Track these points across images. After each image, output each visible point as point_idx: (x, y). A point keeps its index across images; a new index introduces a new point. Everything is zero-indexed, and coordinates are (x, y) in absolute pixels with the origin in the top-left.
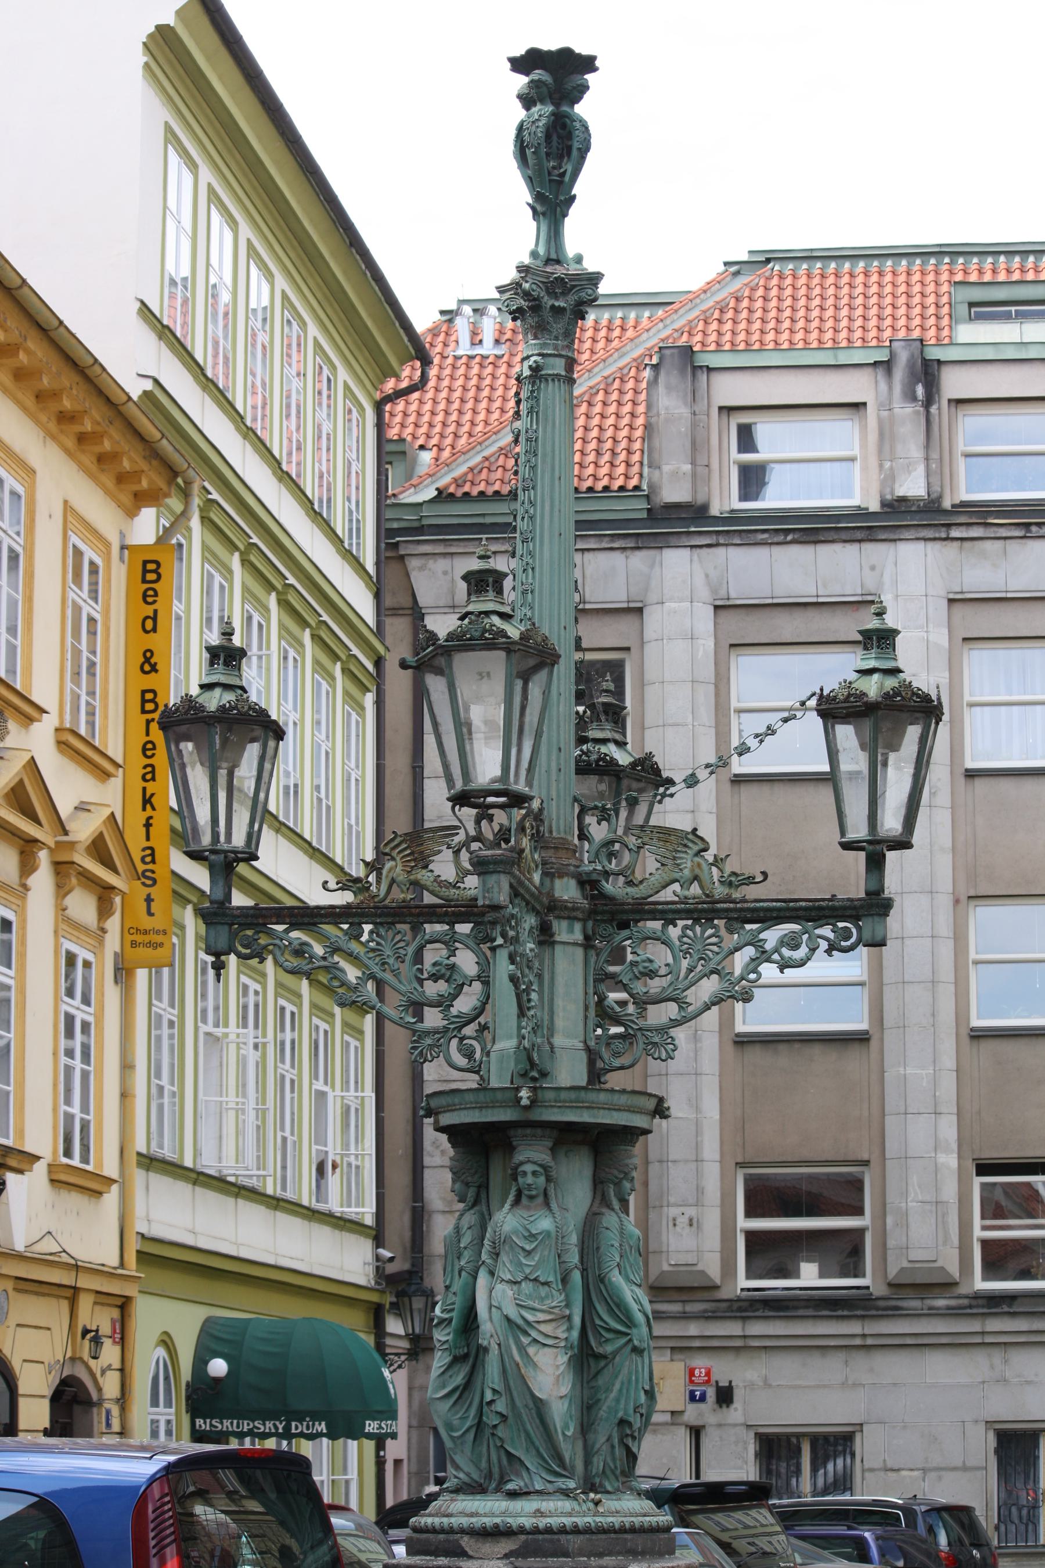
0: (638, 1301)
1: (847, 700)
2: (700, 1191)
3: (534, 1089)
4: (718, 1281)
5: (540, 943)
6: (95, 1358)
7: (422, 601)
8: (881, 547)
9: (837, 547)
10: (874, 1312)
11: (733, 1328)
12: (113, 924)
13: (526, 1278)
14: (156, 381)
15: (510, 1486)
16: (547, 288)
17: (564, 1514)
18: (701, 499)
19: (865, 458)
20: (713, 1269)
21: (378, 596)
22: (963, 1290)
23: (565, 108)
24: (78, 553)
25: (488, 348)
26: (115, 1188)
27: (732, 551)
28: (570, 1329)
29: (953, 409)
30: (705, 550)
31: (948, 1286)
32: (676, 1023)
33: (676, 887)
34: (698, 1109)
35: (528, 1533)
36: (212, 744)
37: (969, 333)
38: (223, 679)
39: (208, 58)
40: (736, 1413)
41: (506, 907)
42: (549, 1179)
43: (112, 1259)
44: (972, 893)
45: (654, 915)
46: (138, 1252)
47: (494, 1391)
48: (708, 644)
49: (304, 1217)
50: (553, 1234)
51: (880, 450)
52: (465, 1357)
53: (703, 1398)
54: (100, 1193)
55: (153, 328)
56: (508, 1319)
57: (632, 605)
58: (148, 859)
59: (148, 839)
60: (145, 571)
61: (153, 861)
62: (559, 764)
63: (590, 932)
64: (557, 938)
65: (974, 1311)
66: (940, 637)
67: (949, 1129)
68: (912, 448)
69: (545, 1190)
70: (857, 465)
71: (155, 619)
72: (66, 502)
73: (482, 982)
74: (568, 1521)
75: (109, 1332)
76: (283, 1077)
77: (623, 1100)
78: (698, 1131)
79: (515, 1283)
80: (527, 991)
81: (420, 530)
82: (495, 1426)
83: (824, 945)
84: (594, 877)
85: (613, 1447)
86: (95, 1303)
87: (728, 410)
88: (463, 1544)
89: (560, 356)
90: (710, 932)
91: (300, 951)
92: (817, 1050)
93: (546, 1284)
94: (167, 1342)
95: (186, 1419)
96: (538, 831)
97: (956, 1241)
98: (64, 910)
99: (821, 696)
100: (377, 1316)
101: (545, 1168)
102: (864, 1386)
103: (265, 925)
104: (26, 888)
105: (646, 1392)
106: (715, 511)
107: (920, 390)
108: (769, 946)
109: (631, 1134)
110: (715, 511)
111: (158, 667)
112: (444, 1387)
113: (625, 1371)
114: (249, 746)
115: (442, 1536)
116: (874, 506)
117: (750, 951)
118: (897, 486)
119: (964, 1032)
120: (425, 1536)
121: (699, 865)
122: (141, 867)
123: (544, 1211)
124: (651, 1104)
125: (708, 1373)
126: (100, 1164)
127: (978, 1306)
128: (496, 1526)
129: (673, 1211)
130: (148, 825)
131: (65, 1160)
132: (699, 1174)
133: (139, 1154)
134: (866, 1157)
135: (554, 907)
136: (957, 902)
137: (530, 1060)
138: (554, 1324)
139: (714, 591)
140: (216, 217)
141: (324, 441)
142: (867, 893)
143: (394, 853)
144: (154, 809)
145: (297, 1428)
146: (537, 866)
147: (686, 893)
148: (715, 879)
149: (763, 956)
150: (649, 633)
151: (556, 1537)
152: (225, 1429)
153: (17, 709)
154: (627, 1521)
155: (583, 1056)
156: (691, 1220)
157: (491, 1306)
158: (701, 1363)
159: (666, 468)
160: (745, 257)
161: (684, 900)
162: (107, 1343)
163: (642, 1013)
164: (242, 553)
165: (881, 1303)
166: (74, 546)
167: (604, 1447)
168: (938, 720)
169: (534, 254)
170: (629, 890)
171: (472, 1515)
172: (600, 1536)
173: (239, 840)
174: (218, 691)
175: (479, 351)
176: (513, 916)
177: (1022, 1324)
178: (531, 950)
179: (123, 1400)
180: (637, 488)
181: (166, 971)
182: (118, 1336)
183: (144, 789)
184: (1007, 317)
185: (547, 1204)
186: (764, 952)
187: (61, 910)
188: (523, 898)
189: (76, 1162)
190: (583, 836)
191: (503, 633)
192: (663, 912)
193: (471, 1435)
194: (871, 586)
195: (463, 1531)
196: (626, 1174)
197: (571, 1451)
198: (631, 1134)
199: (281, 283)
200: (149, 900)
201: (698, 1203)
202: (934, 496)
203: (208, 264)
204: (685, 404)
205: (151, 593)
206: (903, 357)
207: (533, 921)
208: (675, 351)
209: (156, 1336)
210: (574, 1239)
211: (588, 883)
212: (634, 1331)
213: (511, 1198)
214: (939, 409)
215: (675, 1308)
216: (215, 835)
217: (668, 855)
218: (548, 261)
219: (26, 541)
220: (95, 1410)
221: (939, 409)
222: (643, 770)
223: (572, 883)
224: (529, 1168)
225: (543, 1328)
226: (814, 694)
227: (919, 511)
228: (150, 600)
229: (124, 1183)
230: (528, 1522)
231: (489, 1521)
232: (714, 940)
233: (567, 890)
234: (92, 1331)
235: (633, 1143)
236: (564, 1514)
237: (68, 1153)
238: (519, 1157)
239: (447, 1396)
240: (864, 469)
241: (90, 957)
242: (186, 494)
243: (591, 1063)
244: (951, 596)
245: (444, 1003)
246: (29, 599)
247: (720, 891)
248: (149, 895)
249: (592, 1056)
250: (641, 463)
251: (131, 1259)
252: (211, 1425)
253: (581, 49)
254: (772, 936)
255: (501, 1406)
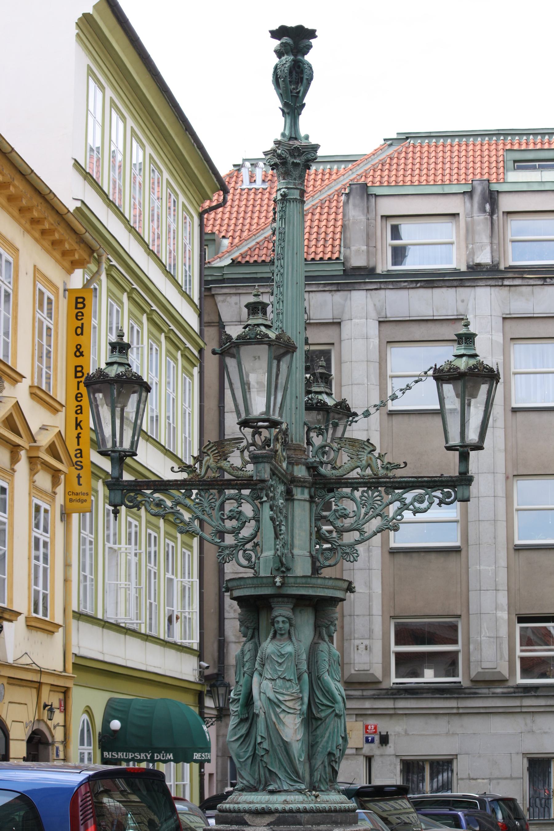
0: (338, 690)
1: (449, 371)
2: (371, 631)
3: (283, 577)
4: (381, 679)
5: (287, 500)
6: (51, 720)
7: (224, 319)
8: (467, 290)
9: (444, 290)
10: (463, 696)
11: (389, 704)
12: (60, 490)
13: (279, 677)
14: (83, 202)
15: (271, 788)
16: (290, 153)
17: (299, 802)
18: (371, 265)
19: (458, 243)
20: (378, 673)
21: (200, 316)
22: (511, 684)
23: (300, 57)
24: (41, 293)
25: (259, 185)
26: (61, 629)
27: (388, 292)
28: (302, 704)
29: (505, 217)
30: (374, 292)
31: (502, 681)
32: (358, 542)
33: (358, 470)
34: (370, 588)
35: (280, 813)
36: (112, 395)
37: (514, 176)
38: (118, 360)
39: (110, 31)
40: (390, 749)
41: (268, 481)
42: (291, 625)
43: (59, 667)
44: (515, 473)
45: (347, 485)
46: (73, 663)
47: (262, 737)
48: (375, 341)
49: (161, 645)
50: (293, 654)
51: (467, 239)
52: (247, 719)
53: (373, 741)
54: (53, 632)
55: (81, 174)
56: (269, 699)
57: (335, 321)
58: (79, 455)
59: (78, 445)
60: (77, 303)
61: (81, 457)
62: (296, 405)
63: (313, 494)
64: (295, 497)
65: (517, 695)
66: (499, 337)
67: (503, 598)
68: (484, 237)
69: (289, 631)
70: (455, 246)
71: (82, 328)
72: (35, 266)
73: (256, 521)
74: (301, 806)
75: (58, 706)
76: (150, 571)
77: (330, 583)
78: (370, 600)
79: (273, 680)
80: (280, 525)
81: (223, 281)
82: (262, 756)
83: (437, 501)
84: (315, 465)
85: (325, 767)
86: (51, 691)
87: (386, 217)
88: (246, 818)
89: (297, 189)
90: (376, 494)
91: (159, 504)
92: (433, 556)
93: (290, 680)
94: (88, 711)
95: (98, 752)
96: (285, 441)
97: (507, 658)
98: (34, 482)
99: (435, 369)
100: (200, 697)
101: (289, 619)
102: (458, 734)
103: (140, 490)
104: (14, 470)
105: (342, 738)
106: (379, 271)
107: (488, 207)
108: (407, 501)
109: (335, 601)
110: (379, 271)
111: (84, 354)
112: (235, 735)
113: (331, 727)
114: (132, 395)
115: (234, 814)
116: (464, 268)
117: (397, 504)
118: (475, 257)
119: (511, 547)
120: (225, 814)
121: (371, 458)
122: (75, 460)
123: (288, 642)
124: (345, 585)
125: (375, 728)
126: (53, 617)
127: (518, 692)
128: (263, 809)
129: (357, 642)
130: (78, 437)
131: (34, 615)
132: (370, 622)
133: (74, 612)
134: (459, 613)
135: (294, 481)
136: (507, 478)
137: (281, 562)
138: (293, 702)
139: (378, 313)
140: (114, 115)
141: (172, 234)
142: (460, 473)
143: (209, 452)
144: (81, 429)
145: (157, 757)
146: (285, 459)
147: (364, 473)
148: (379, 466)
149: (405, 507)
150: (344, 335)
151: (295, 814)
152: (119, 757)
153: (9, 376)
154: (333, 806)
155: (309, 560)
156: (366, 647)
157: (260, 692)
158: (372, 722)
159: (353, 248)
160: (395, 136)
161: (363, 477)
162: (57, 712)
163: (340, 537)
164: (128, 293)
165: (467, 691)
166: (39, 289)
167: (320, 767)
168: (498, 382)
169: (283, 135)
170: (334, 471)
171: (250, 803)
172: (318, 814)
173: (126, 445)
174: (115, 366)
175: (254, 186)
176: (272, 485)
177: (542, 702)
178: (282, 503)
179: (65, 742)
180: (337, 259)
181: (88, 514)
182: (62, 708)
183: (77, 418)
184: (534, 168)
185: (290, 638)
186: (405, 505)
187: (32, 482)
188: (278, 476)
189: (40, 616)
190: (309, 443)
191: (267, 336)
192: (352, 483)
193: (250, 761)
194: (462, 311)
195: (245, 811)
196: (332, 622)
197: (303, 769)
198: (335, 601)
199: (149, 150)
200: (79, 477)
201: (370, 638)
202: (495, 263)
203: (110, 140)
204: (363, 214)
205: (80, 314)
206: (479, 189)
207: (282, 488)
208: (358, 186)
209: (82, 708)
210: (304, 657)
211: (312, 468)
212: (336, 705)
213: (271, 635)
214: (498, 217)
215: (358, 693)
216: (114, 443)
217: (354, 453)
218: (291, 138)
219: (14, 286)
220: (50, 747)
221: (498, 217)
222: (341, 408)
223: (304, 468)
224: (280, 619)
225: (288, 704)
226: (431, 368)
227: (487, 271)
228: (79, 318)
229: (66, 627)
230: (280, 807)
231: (259, 806)
232: (378, 498)
233: (301, 472)
234: (49, 705)
235: (335, 606)
236: (299, 802)
237: (36, 611)
238: (275, 613)
239: (237, 740)
240: (458, 248)
241: (48, 507)
242: (98, 262)
243: (313, 563)
244: (504, 316)
245: (235, 532)
246: (15, 318)
247: (381, 472)
248: (79, 474)
249: (314, 560)
250: (340, 245)
251: (70, 667)
252: (112, 755)
253: (308, 26)
254: (409, 496)
255: (265, 745)
